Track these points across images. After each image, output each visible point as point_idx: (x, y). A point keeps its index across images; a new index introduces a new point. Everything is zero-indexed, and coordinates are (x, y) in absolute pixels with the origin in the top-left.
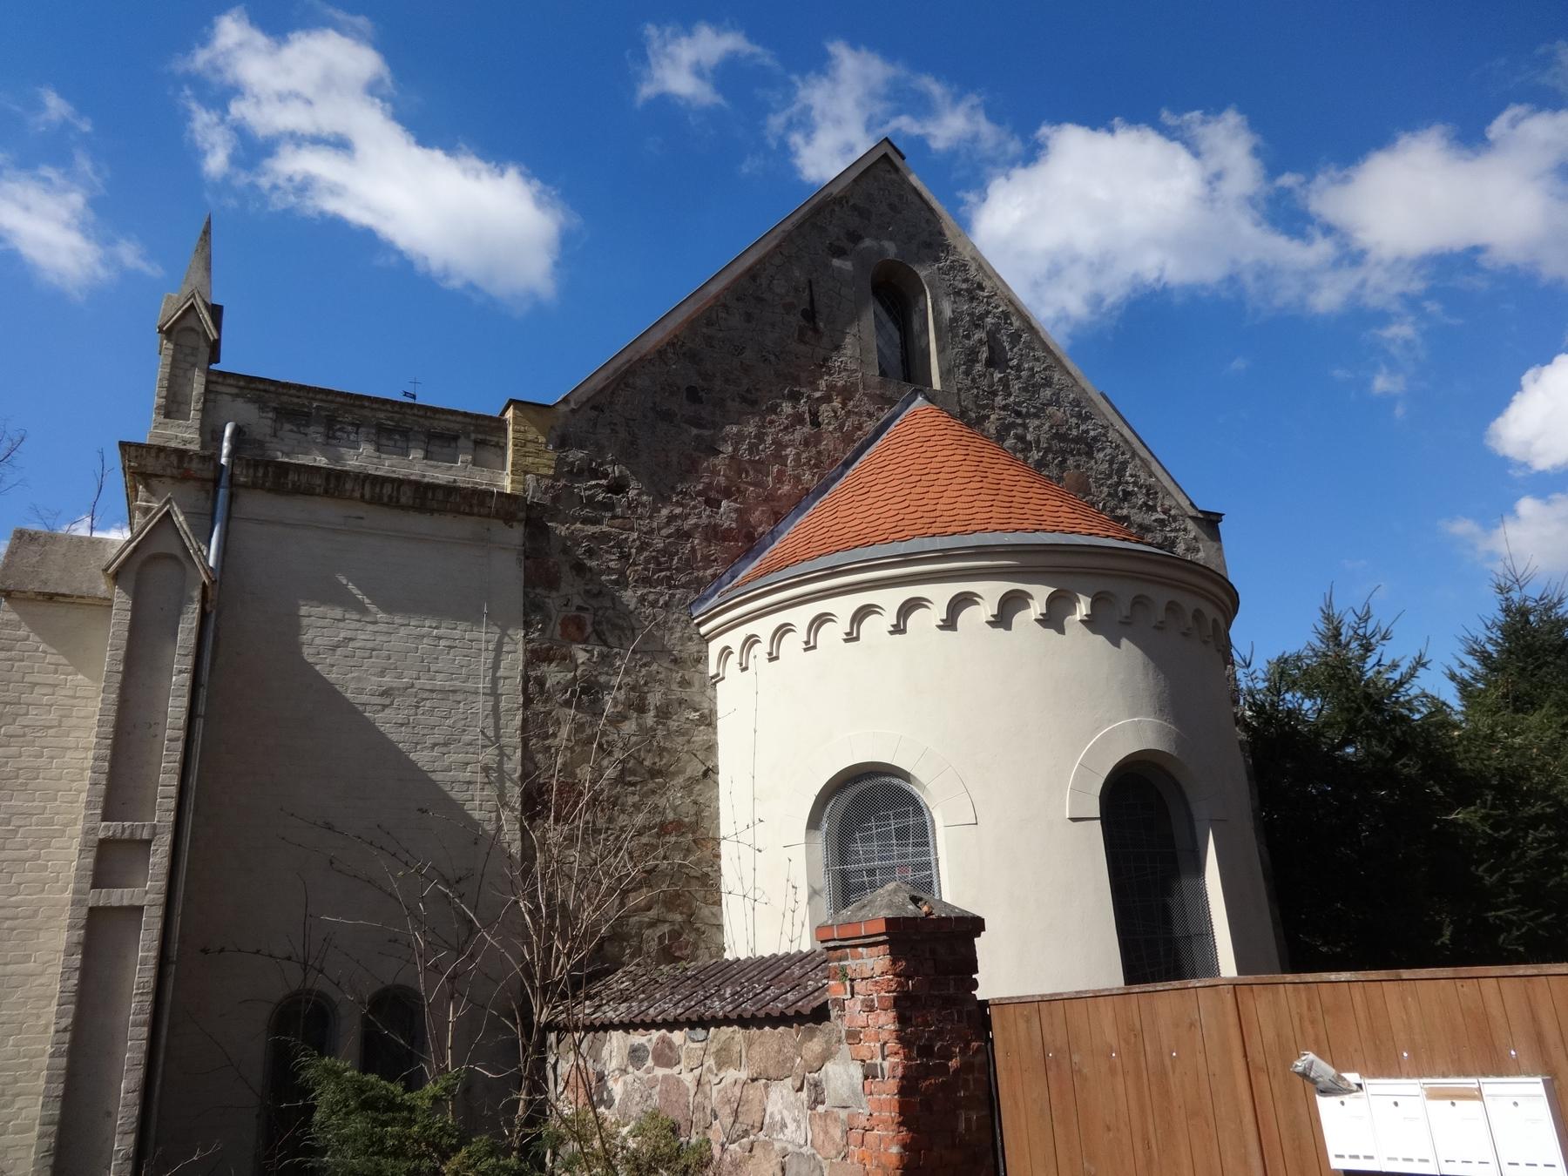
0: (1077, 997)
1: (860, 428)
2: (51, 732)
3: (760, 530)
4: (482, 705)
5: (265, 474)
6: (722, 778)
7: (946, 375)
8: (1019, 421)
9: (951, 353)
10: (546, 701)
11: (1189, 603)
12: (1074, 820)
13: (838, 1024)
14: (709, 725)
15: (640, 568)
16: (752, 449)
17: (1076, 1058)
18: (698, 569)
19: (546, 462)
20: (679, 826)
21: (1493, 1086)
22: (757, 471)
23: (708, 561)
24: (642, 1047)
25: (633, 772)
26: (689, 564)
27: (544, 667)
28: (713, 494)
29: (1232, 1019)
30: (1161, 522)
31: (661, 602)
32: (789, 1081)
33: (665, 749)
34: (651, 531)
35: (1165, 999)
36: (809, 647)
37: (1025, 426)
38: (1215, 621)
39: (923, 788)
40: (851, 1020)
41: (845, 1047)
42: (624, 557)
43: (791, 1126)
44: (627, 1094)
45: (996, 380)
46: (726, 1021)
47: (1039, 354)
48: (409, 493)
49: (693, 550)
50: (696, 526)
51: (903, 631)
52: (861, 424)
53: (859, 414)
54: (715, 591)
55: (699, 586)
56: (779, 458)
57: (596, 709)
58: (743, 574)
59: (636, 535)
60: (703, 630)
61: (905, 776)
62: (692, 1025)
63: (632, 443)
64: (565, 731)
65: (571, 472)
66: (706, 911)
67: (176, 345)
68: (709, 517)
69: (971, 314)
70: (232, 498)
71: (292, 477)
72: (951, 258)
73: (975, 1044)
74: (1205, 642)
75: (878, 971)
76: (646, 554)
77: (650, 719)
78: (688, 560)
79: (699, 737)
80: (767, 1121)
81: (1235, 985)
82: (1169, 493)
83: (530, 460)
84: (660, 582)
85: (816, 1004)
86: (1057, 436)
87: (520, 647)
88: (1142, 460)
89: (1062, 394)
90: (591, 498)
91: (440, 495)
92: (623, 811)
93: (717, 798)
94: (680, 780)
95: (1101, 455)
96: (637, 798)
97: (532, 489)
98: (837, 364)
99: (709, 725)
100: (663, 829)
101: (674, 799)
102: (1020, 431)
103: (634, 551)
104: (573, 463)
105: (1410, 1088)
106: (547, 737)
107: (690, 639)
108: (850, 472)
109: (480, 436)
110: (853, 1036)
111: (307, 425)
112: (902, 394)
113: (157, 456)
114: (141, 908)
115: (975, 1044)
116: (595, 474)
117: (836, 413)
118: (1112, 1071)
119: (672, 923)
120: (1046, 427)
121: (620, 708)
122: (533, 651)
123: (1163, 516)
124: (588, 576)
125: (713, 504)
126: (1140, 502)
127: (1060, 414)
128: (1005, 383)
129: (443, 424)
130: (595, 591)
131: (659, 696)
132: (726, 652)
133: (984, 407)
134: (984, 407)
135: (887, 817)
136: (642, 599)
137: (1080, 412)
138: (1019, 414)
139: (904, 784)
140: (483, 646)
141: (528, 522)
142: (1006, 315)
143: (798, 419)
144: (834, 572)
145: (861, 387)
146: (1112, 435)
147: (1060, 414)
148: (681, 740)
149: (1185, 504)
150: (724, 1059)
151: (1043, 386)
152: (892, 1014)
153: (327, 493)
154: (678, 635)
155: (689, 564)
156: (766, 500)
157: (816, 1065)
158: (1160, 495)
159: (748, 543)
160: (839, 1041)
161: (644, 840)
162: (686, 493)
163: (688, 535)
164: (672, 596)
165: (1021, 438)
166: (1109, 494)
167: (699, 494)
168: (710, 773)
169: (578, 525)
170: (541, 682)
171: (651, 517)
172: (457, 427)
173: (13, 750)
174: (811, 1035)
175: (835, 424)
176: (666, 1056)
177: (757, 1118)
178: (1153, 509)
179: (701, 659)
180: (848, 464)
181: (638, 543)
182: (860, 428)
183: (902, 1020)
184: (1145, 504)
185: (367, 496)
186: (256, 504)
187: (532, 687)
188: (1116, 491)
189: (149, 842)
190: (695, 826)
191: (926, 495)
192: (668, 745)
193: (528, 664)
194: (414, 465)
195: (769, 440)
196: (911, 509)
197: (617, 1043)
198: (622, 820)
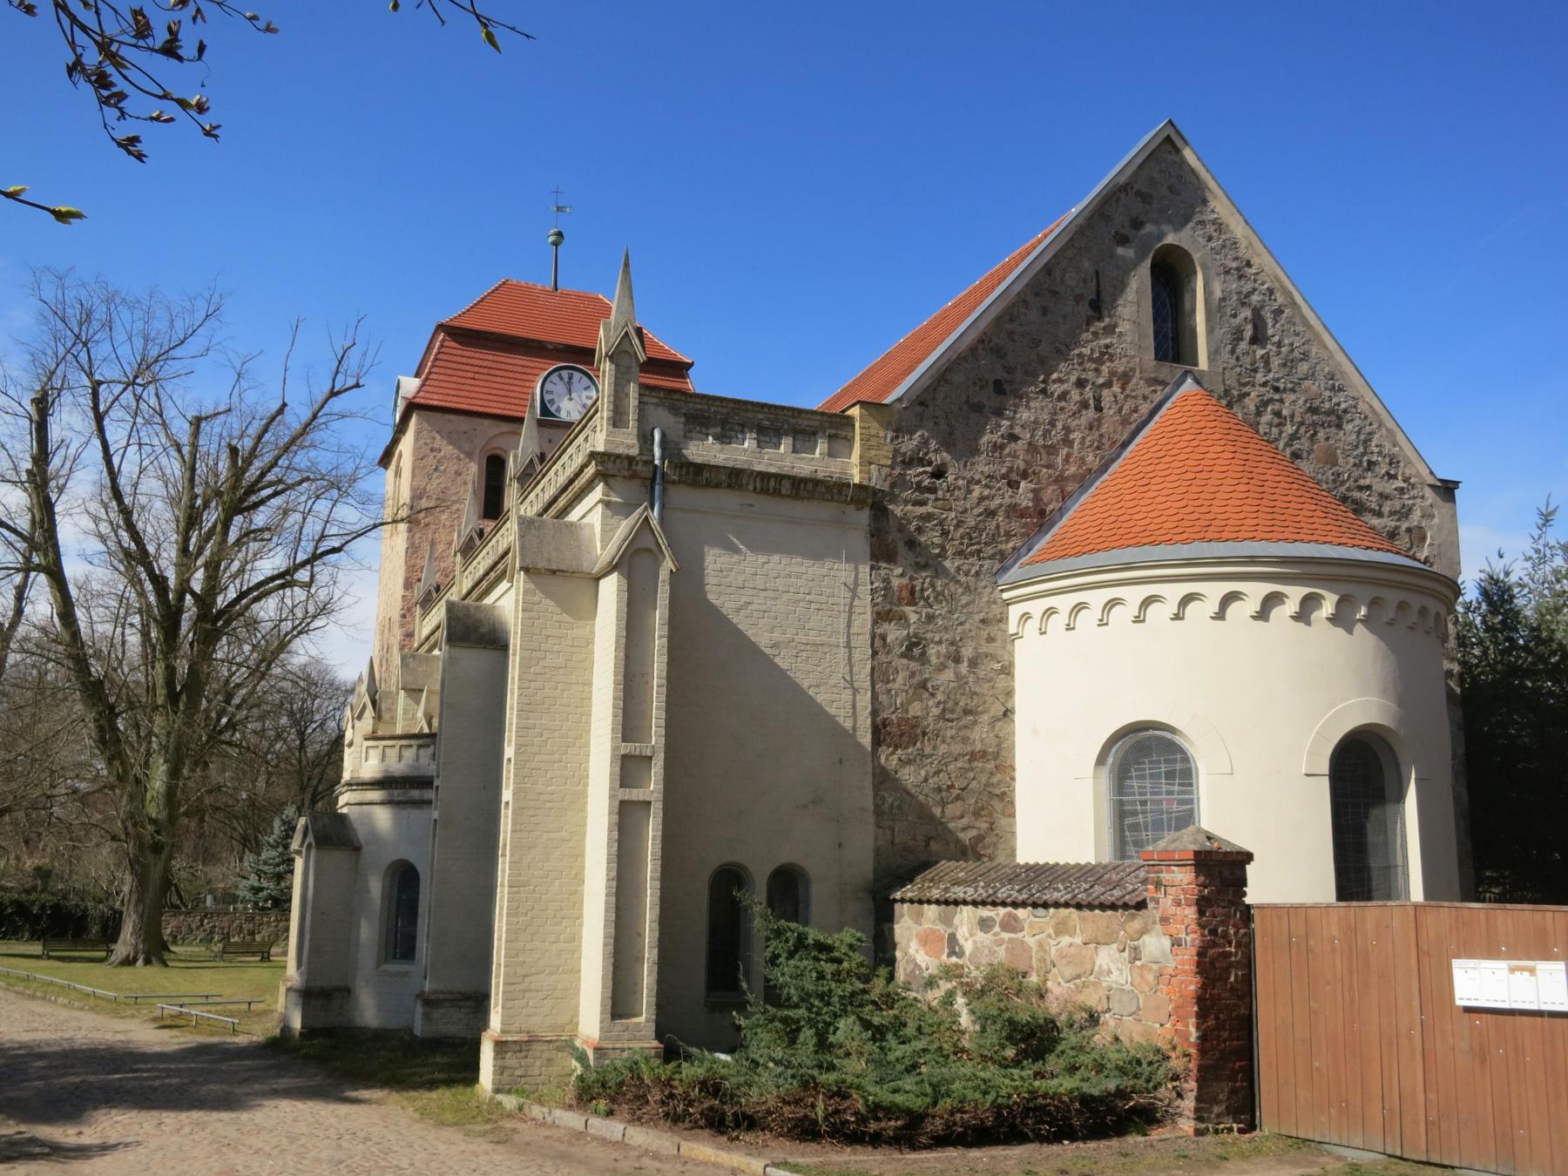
0: (1314, 907)
1: (1136, 410)
2: (562, 671)
3: (1051, 507)
4: (842, 653)
5: (687, 473)
6: (1018, 717)
7: (1213, 355)
8: (1277, 397)
9: (1222, 332)
10: (888, 653)
11: (1416, 601)
12: (1307, 775)
13: (1153, 912)
14: (1008, 674)
15: (957, 543)
16: (1047, 433)
17: (1311, 942)
18: (1001, 542)
19: (884, 455)
20: (984, 754)
21: (1541, 966)
22: (1049, 453)
23: (1009, 535)
24: (992, 919)
25: (953, 711)
26: (993, 540)
27: (886, 626)
28: (1014, 476)
29: (1412, 925)
30: (1401, 490)
31: (973, 572)
32: (1115, 946)
33: (976, 693)
34: (965, 511)
35: (1369, 913)
36: (1102, 623)
37: (1281, 401)
38: (1438, 614)
39: (1191, 743)
40: (1164, 910)
41: (1158, 927)
42: (945, 533)
43: (1116, 973)
44: (976, 949)
45: (1258, 357)
46: (1067, 905)
47: (1300, 328)
48: (788, 486)
49: (998, 526)
50: (1001, 505)
51: (1183, 618)
52: (1137, 407)
53: (1135, 397)
54: (1015, 562)
55: (1004, 560)
56: (1068, 442)
57: (923, 658)
58: (1037, 547)
59: (953, 515)
60: (1006, 596)
61: (1172, 730)
62: (1035, 905)
63: (951, 434)
64: (900, 679)
65: (903, 462)
66: (1004, 821)
67: (617, 365)
68: (1011, 497)
69: (1239, 293)
70: (664, 491)
71: (706, 474)
72: (1223, 237)
73: (1242, 931)
74: (1427, 633)
75: (1185, 882)
76: (961, 530)
77: (964, 668)
78: (993, 535)
79: (1001, 682)
80: (1096, 969)
81: (1416, 906)
82: (1410, 462)
83: (873, 452)
84: (972, 554)
85: (1139, 899)
86: (1313, 410)
87: (869, 610)
88: (1388, 430)
89: (1318, 368)
90: (919, 484)
91: (810, 487)
92: (944, 741)
93: (1014, 733)
94: (985, 718)
95: (1350, 427)
96: (954, 732)
97: (877, 480)
98: (1119, 351)
99: (1008, 674)
100: (973, 756)
101: (980, 735)
102: (1277, 406)
103: (952, 528)
104: (905, 454)
105: (1501, 966)
106: (888, 682)
107: (995, 602)
108: (1126, 453)
109: (833, 432)
110: (1164, 920)
111: (707, 428)
112: (1174, 376)
113: (615, 462)
114: (649, 803)
115: (1242, 931)
116: (922, 462)
117: (1115, 396)
118: (1334, 950)
119: (979, 829)
120: (1301, 402)
121: (942, 659)
122: (878, 613)
123: (1405, 485)
124: (918, 550)
125: (1014, 485)
126: (1383, 471)
127: (1315, 388)
128: (1266, 359)
129: (806, 422)
130: (923, 563)
131: (970, 650)
132: (1026, 616)
133: (1245, 385)
134: (1245, 385)
135: (1159, 762)
136: (958, 569)
137: (1334, 386)
138: (1277, 390)
139: (1168, 735)
140: (842, 609)
141: (872, 507)
142: (1271, 291)
143: (1084, 405)
144: (1128, 567)
145: (1138, 371)
146: (1362, 407)
147: (1315, 388)
148: (987, 685)
149: (1425, 472)
150: (1061, 929)
151: (1301, 360)
152: (1194, 908)
153: (729, 486)
154: (985, 599)
155: (993, 540)
156: (1056, 481)
157: (1136, 936)
158: (1402, 464)
159: (1041, 518)
160: (1154, 923)
161: (960, 764)
162: (992, 477)
163: (992, 514)
164: (982, 566)
165: (1278, 414)
166: (1355, 465)
167: (1003, 477)
168: (1008, 713)
169: (909, 507)
170: (883, 638)
171: (965, 499)
172: (816, 424)
173: (539, 684)
174: (1133, 917)
175: (1115, 408)
176: (1010, 925)
177: (1089, 967)
178: (1393, 477)
179: (1003, 619)
180: (1125, 445)
181: (955, 522)
182: (1136, 410)
183: (1201, 913)
184: (1388, 473)
185: (758, 488)
186: (683, 496)
187: (878, 643)
188: (1361, 461)
189: (650, 758)
190: (996, 756)
191: (1201, 495)
192: (977, 690)
193: (875, 623)
194: (782, 458)
195: (1060, 425)
196: (1189, 509)
197: (966, 912)
198: (943, 749)
